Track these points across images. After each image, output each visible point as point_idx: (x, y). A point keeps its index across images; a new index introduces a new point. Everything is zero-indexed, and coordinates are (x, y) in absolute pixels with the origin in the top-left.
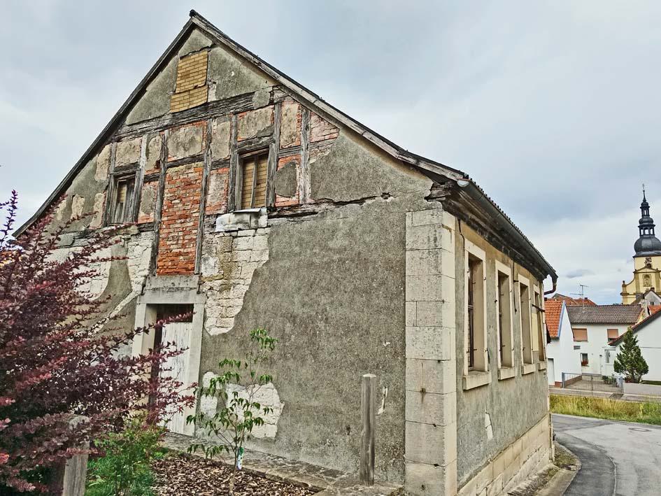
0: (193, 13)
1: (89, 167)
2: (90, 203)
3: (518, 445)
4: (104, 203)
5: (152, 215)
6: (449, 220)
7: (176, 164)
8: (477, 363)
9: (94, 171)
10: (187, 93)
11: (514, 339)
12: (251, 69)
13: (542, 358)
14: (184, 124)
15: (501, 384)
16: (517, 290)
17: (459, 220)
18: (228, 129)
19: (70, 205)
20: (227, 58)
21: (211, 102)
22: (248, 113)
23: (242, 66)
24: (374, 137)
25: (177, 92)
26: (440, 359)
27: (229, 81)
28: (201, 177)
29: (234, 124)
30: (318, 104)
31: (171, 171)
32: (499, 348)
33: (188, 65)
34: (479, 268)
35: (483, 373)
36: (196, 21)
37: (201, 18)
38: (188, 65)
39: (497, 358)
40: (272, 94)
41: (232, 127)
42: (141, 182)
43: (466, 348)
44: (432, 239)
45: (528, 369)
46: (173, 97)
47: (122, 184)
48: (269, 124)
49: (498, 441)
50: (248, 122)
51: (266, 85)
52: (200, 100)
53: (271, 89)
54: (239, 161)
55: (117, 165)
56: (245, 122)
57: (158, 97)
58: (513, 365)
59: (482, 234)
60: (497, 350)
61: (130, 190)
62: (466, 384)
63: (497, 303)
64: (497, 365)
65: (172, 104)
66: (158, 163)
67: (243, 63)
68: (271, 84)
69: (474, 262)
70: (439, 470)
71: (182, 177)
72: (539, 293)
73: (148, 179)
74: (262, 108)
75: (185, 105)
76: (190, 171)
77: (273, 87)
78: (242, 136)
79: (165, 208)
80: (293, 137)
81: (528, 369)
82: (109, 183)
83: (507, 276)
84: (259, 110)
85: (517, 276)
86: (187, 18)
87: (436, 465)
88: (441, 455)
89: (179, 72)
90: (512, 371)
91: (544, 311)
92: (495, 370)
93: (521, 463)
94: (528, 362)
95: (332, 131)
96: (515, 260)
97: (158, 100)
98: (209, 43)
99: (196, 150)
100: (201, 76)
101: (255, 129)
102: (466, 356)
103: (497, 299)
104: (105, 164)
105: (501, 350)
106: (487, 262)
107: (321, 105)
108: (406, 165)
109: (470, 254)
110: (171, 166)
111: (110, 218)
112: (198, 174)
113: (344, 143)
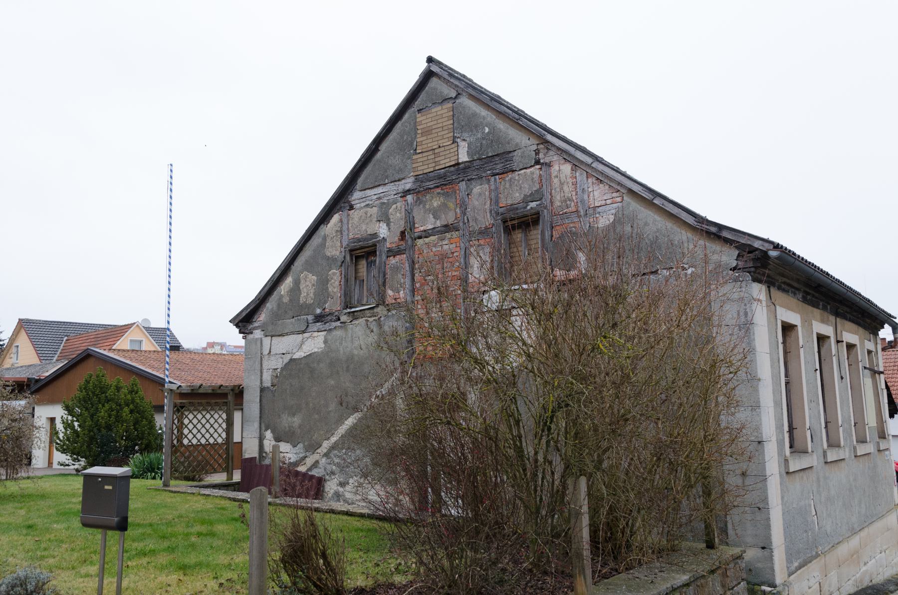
0: (430, 60)
1: (316, 241)
2: (323, 282)
3: (855, 542)
4: (340, 282)
5: (402, 293)
6: (758, 290)
7: (426, 234)
8: (797, 444)
9: (323, 245)
10: (431, 153)
11: (843, 412)
12: (509, 124)
13: (882, 435)
14: (430, 189)
15: (827, 466)
16: (843, 351)
17: (769, 287)
18: (487, 193)
19: (297, 282)
20: (478, 111)
21: (463, 163)
22: (510, 175)
23: (497, 120)
24: (666, 203)
25: (418, 151)
26: (760, 440)
27: (483, 139)
28: (458, 249)
29: (493, 187)
30: (595, 165)
31: (420, 242)
32: (823, 425)
33: (430, 120)
34: (793, 334)
35: (808, 454)
36: (435, 68)
37: (439, 63)
38: (430, 120)
39: (821, 437)
40: (537, 152)
41: (490, 191)
42: (384, 257)
43: (786, 428)
44: (742, 314)
45: (862, 450)
46: (415, 157)
47: (358, 258)
48: (538, 186)
49: (829, 533)
50: (510, 185)
51: (529, 142)
52: (448, 160)
53: (535, 147)
54: (504, 230)
55: (351, 236)
56: (507, 185)
57: (395, 158)
58: (842, 443)
59: (795, 294)
60: (821, 428)
61: (370, 264)
62: (788, 466)
63: (818, 372)
64: (822, 445)
65: (414, 166)
66: (403, 234)
67: (497, 117)
68: (534, 141)
69: (788, 328)
70: (766, 552)
71: (434, 249)
72: (874, 350)
73: (392, 253)
74: (526, 168)
75: (430, 166)
76: (444, 243)
77: (538, 144)
78: (503, 203)
79: (418, 285)
80: (568, 202)
81: (862, 450)
82: (344, 257)
83: (829, 337)
84: (522, 171)
85: (842, 335)
86: (424, 65)
87: (763, 548)
88: (768, 537)
89: (418, 127)
90: (841, 451)
91: (882, 373)
92: (821, 452)
93: (862, 564)
94: (862, 441)
95: (615, 195)
96: (837, 314)
97: (396, 161)
98: (453, 94)
99: (450, 218)
100: (446, 132)
101: (520, 194)
102: (787, 436)
103: (818, 367)
104: (337, 236)
105: (826, 427)
106: (803, 326)
107: (601, 167)
108: (709, 234)
109: (783, 322)
110: (420, 238)
111: (350, 298)
112: (454, 245)
113: (631, 209)
